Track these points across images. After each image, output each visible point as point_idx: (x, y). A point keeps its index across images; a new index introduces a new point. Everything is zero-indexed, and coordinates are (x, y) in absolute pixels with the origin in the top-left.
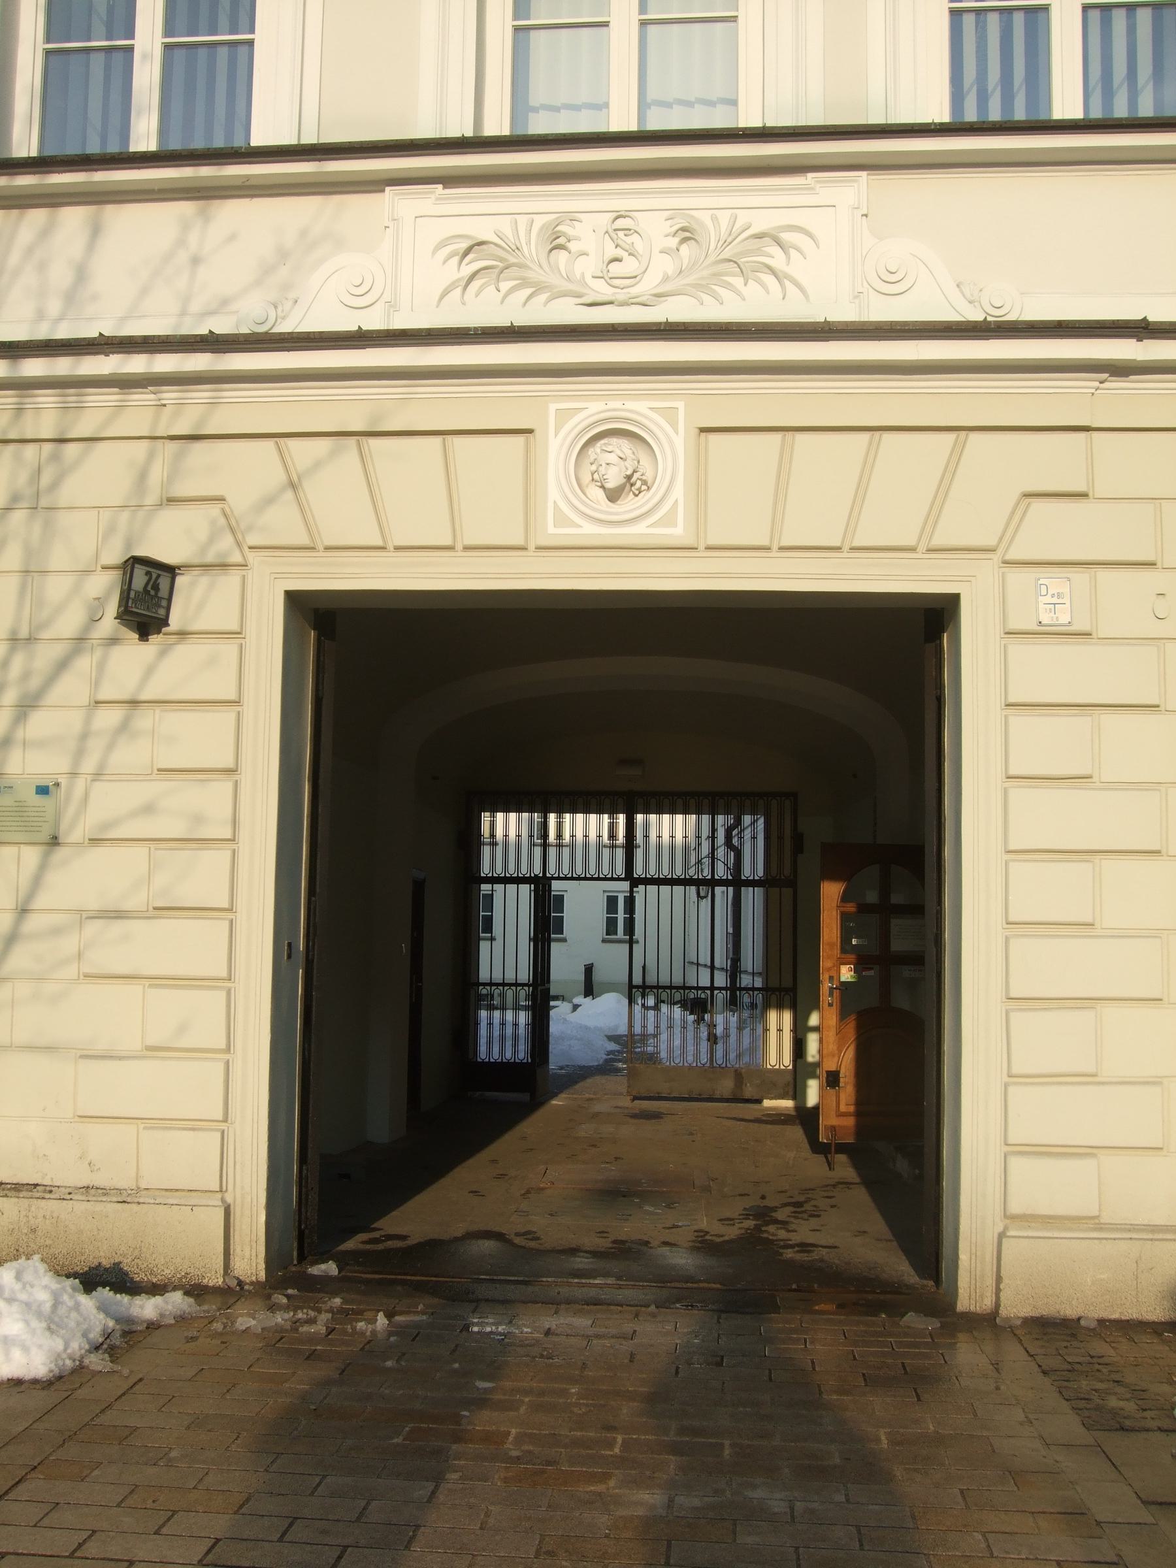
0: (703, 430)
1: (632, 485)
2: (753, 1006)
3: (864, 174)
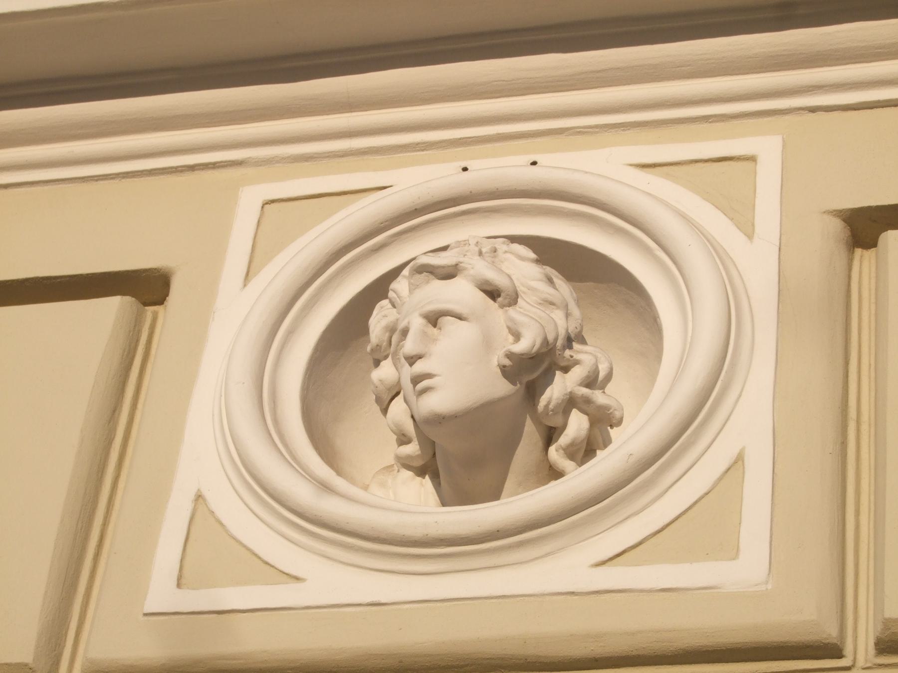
1: (550, 435)
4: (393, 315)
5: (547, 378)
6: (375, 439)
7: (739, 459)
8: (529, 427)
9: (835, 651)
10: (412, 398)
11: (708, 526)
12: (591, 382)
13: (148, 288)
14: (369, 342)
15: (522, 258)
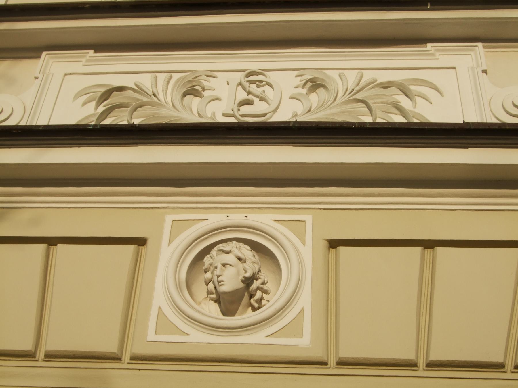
0: (334, 244)
1: (251, 296)
2: (209, 293)
3: (480, 44)
4: (211, 261)
5: (252, 283)
6: (201, 289)
7: (302, 309)
8: (246, 294)
9: (326, 364)
10: (216, 283)
11: (294, 328)
12: (263, 283)
13: (141, 242)
14: (204, 265)
15: (247, 250)
